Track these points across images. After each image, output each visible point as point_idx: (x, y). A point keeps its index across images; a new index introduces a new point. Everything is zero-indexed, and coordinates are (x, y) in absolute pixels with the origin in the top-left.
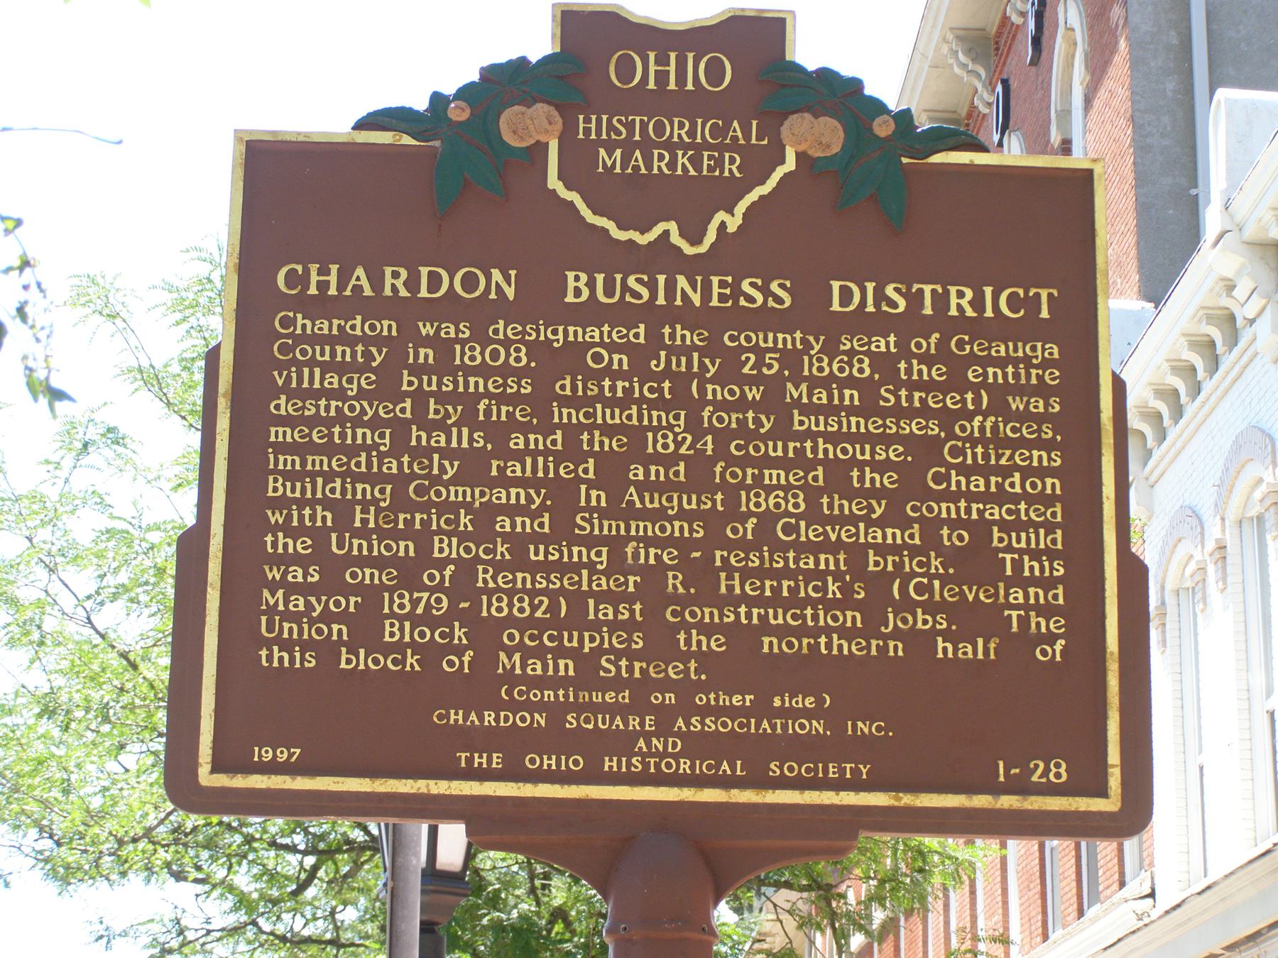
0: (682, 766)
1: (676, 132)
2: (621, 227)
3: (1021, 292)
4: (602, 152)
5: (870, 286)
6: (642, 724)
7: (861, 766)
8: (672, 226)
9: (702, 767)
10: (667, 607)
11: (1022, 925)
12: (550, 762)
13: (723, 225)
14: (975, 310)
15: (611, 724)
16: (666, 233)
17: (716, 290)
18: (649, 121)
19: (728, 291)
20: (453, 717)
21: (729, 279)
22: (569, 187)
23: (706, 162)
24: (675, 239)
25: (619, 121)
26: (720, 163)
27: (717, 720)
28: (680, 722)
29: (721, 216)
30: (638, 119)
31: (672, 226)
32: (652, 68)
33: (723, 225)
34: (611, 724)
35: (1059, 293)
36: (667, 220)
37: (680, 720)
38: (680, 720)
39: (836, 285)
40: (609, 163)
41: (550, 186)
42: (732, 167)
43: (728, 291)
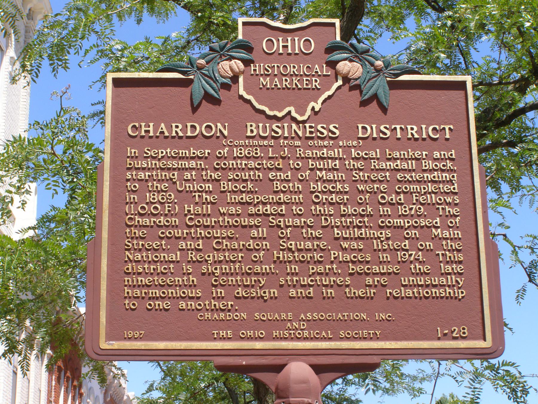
0: (305, 334)
1: (292, 70)
2: (271, 109)
3: (437, 127)
4: (261, 79)
5: (374, 126)
6: (287, 316)
7: (377, 332)
8: (292, 109)
9: (313, 334)
10: (127, 126)
11: (84, 343)
12: (250, 333)
13: (313, 108)
14: (418, 135)
15: (273, 317)
16: (289, 112)
17: (308, 130)
18: (281, 66)
19: (313, 130)
20: (207, 316)
21: (313, 125)
22: (248, 93)
23: (305, 82)
24: (294, 114)
25: (268, 66)
26: (310, 82)
27: (345, 332)
28: (302, 316)
29: (312, 104)
30: (276, 65)
31: (292, 109)
32: (281, 44)
33: (313, 108)
34: (273, 317)
35: (454, 126)
36: (290, 106)
37: (302, 315)
38: (302, 315)
39: (360, 126)
40: (265, 83)
41: (240, 94)
42: (316, 83)
43: (313, 130)
